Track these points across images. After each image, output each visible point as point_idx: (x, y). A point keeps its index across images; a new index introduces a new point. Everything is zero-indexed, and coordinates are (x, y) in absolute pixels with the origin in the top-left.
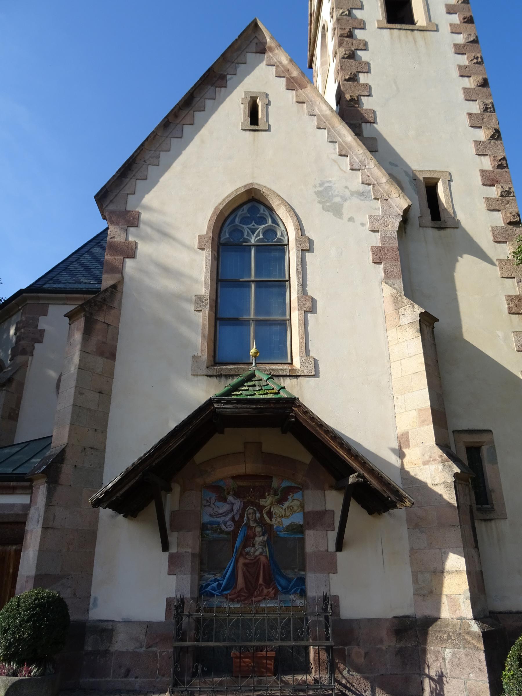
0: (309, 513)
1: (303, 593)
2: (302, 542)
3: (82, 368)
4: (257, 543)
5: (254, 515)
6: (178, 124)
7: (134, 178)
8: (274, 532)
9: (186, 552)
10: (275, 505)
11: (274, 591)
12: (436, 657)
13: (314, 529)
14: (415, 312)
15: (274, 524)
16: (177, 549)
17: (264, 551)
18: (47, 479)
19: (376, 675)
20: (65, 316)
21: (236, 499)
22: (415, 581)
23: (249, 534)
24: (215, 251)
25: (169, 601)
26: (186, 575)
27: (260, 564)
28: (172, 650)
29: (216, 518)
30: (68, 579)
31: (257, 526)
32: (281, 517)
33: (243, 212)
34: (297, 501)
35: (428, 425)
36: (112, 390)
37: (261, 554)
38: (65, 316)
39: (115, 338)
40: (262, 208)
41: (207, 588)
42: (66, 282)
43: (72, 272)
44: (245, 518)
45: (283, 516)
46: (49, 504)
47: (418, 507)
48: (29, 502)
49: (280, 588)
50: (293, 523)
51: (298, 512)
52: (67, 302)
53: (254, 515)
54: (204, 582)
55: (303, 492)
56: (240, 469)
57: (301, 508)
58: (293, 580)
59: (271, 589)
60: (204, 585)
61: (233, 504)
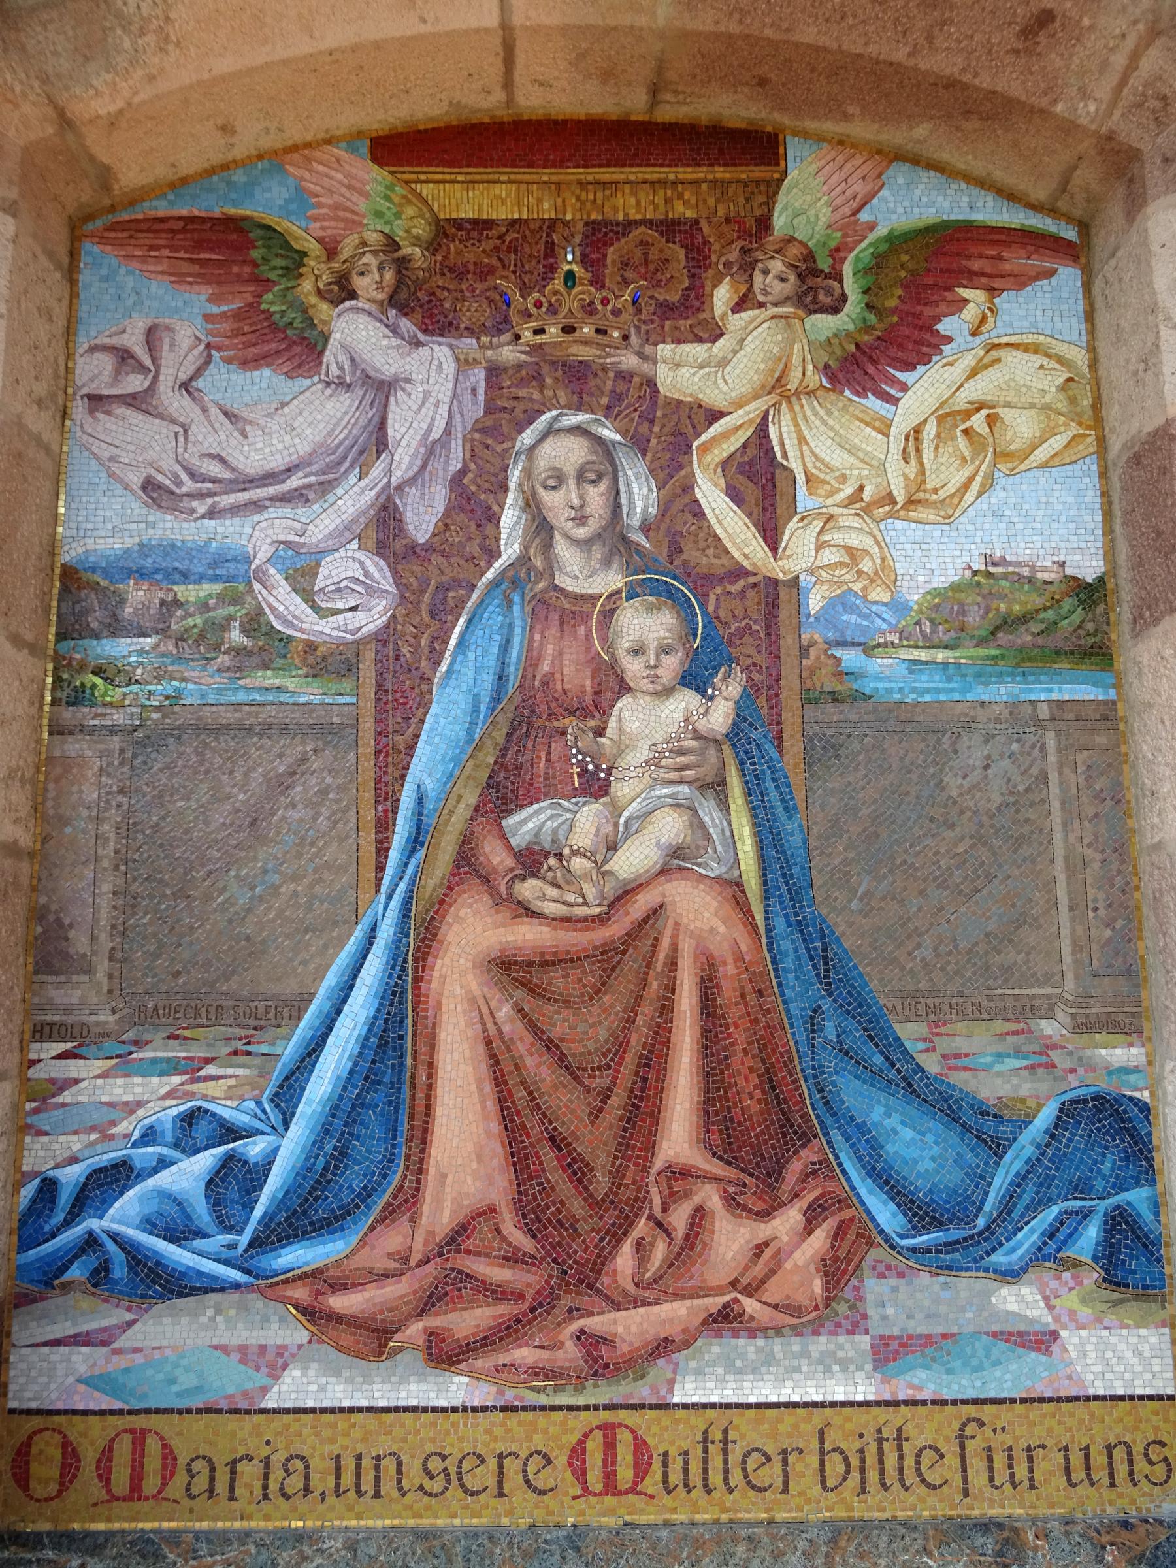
4: (638, 755)
5: (596, 497)
11: (820, 1239)
17: (708, 837)
23: (545, 667)
27: (672, 965)
29: (211, 514)
34: (1038, 360)
44: (510, 517)
45: (890, 499)
50: (1003, 562)
51: (1044, 466)
54: (76, 1144)
57: (1075, 430)
59: (791, 1218)
60: (71, 1176)
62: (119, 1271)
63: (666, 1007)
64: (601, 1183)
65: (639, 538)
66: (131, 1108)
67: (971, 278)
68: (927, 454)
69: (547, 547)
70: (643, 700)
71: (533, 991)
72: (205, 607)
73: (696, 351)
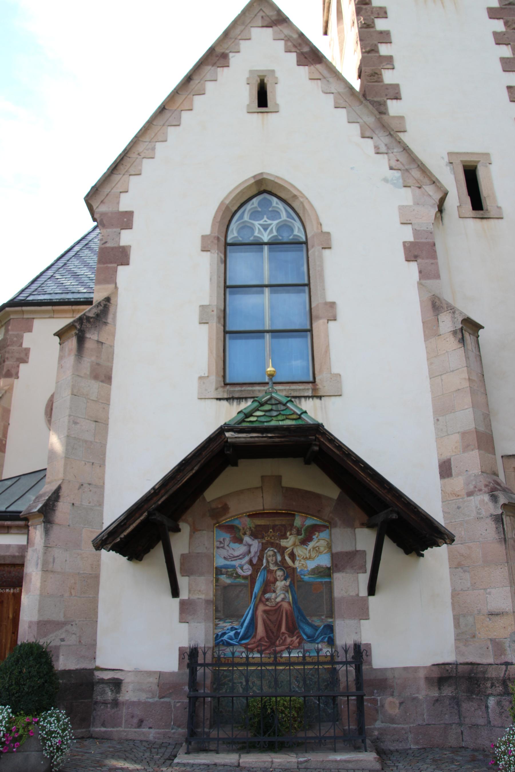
0: (337, 554)
1: (331, 642)
2: (330, 586)
3: (76, 394)
4: (279, 588)
5: (274, 558)
6: (175, 110)
7: (126, 173)
8: (297, 576)
9: (198, 598)
10: (298, 545)
11: (298, 640)
12: (479, 706)
13: (343, 572)
14: (456, 319)
15: (298, 567)
16: (189, 595)
17: (286, 597)
18: (44, 519)
19: (412, 725)
20: (55, 335)
21: (253, 540)
22: (457, 624)
23: (269, 578)
24: (221, 252)
25: (181, 650)
26: (200, 623)
27: (283, 611)
28: (188, 701)
29: (231, 561)
30: (72, 625)
31: (278, 569)
32: (306, 559)
33: (253, 206)
35: (473, 450)
36: (108, 418)
37: (283, 600)
38: (55, 335)
39: (110, 358)
40: (275, 200)
41: (223, 637)
42: (52, 292)
43: (59, 280)
44: (265, 561)
46: (47, 547)
47: (462, 544)
48: (25, 543)
49: (305, 637)
51: (324, 554)
52: (54, 315)
53: (274, 558)
54: (220, 630)
55: (330, 531)
56: (257, 506)
58: (320, 627)
59: (295, 638)
60: (220, 633)
61: (250, 546)
62: (225, 643)
63: (282, 616)
64: (275, 634)
65: (279, 563)
66: (226, 626)
67: (316, 531)
68: (311, 553)
69: (269, 564)
70: (280, 582)
71: (268, 614)
72: (231, 571)
73: (285, 540)
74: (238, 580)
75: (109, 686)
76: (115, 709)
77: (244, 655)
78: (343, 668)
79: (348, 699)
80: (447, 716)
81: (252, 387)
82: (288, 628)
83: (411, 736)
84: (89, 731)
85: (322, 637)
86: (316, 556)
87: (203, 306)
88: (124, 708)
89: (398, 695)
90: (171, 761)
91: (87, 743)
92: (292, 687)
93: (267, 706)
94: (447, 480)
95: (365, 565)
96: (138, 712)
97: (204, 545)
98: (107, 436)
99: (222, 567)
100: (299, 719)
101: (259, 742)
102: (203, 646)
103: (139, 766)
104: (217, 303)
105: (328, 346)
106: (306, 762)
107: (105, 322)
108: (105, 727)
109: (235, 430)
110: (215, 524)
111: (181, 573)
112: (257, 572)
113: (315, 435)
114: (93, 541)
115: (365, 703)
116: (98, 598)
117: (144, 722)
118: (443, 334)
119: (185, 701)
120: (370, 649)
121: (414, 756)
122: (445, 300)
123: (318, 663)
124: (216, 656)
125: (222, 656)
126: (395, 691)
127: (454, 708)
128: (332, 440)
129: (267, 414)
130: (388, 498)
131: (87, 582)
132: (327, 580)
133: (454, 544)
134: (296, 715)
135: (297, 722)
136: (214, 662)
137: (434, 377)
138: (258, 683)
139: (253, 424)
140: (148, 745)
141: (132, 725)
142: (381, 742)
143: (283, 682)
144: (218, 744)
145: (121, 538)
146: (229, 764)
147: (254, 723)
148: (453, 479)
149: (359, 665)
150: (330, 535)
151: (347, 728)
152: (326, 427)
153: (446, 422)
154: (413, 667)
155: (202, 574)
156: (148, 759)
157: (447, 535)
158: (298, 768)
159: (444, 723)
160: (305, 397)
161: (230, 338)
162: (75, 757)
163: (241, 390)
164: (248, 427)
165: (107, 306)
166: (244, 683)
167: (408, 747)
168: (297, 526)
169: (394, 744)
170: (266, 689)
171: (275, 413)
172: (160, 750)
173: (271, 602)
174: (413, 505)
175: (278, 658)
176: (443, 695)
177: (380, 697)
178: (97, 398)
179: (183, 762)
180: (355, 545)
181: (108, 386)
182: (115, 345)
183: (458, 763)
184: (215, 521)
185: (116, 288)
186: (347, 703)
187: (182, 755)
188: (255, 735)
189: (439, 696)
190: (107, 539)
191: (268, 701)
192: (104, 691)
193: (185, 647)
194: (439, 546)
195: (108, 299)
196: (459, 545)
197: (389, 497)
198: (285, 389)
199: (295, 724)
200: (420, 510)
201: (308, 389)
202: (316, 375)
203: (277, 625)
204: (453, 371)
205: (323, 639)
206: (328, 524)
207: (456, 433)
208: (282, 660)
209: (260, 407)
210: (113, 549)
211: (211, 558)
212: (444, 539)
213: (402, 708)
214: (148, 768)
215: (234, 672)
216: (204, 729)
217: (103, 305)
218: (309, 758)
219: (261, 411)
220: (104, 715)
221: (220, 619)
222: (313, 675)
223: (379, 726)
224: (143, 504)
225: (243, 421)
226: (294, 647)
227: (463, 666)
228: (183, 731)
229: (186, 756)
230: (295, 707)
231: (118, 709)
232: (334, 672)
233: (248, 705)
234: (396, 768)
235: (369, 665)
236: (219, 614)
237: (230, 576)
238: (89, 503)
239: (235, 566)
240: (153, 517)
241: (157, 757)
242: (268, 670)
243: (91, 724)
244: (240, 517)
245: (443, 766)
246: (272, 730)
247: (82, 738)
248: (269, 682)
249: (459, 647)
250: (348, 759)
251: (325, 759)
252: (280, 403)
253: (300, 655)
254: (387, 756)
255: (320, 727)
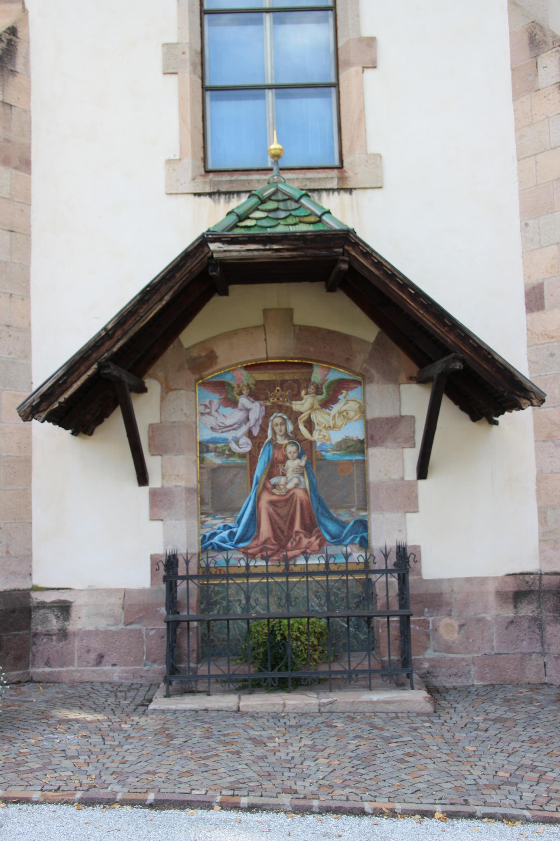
0: (374, 420)
1: (364, 543)
4: (290, 470)
5: (283, 428)
8: (316, 452)
9: (176, 486)
10: (318, 409)
11: (318, 541)
13: (382, 446)
15: (317, 440)
16: (162, 482)
19: (476, 655)
21: (253, 402)
22: (543, 519)
23: (276, 456)
25: (154, 560)
26: (179, 520)
27: (296, 501)
31: (289, 443)
37: (296, 486)
41: (213, 539)
47: (554, 407)
49: (328, 537)
51: (355, 420)
53: (283, 428)
54: (208, 530)
55: (364, 388)
58: (348, 523)
59: (313, 538)
60: (208, 535)
61: (248, 410)
62: (216, 547)
63: (295, 508)
64: (286, 534)
66: (216, 525)
67: (344, 388)
69: (275, 436)
71: (275, 506)
72: (222, 447)
73: (299, 402)
74: (232, 459)
75: (53, 611)
76: (64, 642)
77: (243, 563)
78: (381, 579)
79: (388, 621)
80: (524, 643)
81: (247, 175)
82: (303, 525)
83: (474, 670)
84: (28, 673)
85: (352, 536)
86: (342, 424)
87: (167, 44)
88: (76, 640)
89: (457, 614)
90: (145, 708)
91: (25, 688)
92: (310, 605)
93: (275, 631)
94: (536, 315)
95: (414, 437)
96: (97, 645)
97: (182, 410)
98: (30, 253)
99: (208, 442)
100: (321, 648)
101: (266, 679)
102: (185, 551)
103: (101, 715)
104: (191, 40)
105: (362, 110)
106: (331, 703)
107: (12, 71)
108: (50, 667)
109: (223, 239)
110: (197, 381)
111: (150, 451)
112: (259, 448)
113: (342, 247)
114: (18, 408)
115: (412, 626)
116: (31, 490)
117: (105, 657)
118: (543, 88)
119: (162, 627)
120: (419, 552)
121: (477, 694)
122: (551, 30)
123: (347, 572)
124: (203, 565)
125: (212, 565)
126: (453, 609)
127: (535, 633)
128: (369, 253)
129: (272, 215)
130: (450, 339)
131: (13, 468)
132: (359, 457)
133: (544, 408)
134: (316, 642)
135: (317, 652)
136: (201, 574)
137: (524, 158)
138: (263, 600)
139: (250, 231)
140: (112, 687)
141: (88, 662)
142: (433, 676)
143: (297, 598)
144: (209, 683)
145: (60, 403)
146: (225, 709)
147: (258, 654)
148: (545, 313)
149: (404, 575)
150: (364, 394)
151: (386, 658)
152: (359, 234)
153: (539, 228)
154: (479, 578)
155: (180, 452)
156: (113, 706)
157: (534, 393)
158: (319, 712)
159: (521, 652)
160: (327, 190)
161: (212, 100)
162: (9, 708)
163: (231, 181)
164: (244, 236)
165: (13, 43)
166: (244, 602)
167: (470, 683)
168: (316, 381)
169: (451, 680)
170: (274, 609)
171: (282, 214)
172: (128, 694)
173: (280, 489)
174: (486, 351)
175: (291, 566)
176: (521, 615)
177: (433, 618)
178: (10, 194)
179: (161, 708)
180: (400, 408)
181: (26, 175)
182: (32, 110)
183: (539, 704)
184: (197, 376)
185: (24, 10)
186: (386, 625)
187: (159, 699)
188: (260, 671)
189: (515, 617)
190: (38, 404)
191: (278, 625)
192: (47, 618)
193: (159, 554)
194: (521, 408)
195: (13, 31)
196: (550, 409)
197: (450, 338)
198: (297, 179)
199: (315, 654)
200: (496, 357)
201: (332, 178)
202: (344, 157)
203: (288, 522)
204: (554, 148)
205: (353, 540)
206: (360, 378)
207: (554, 244)
208: (296, 569)
209: (260, 205)
210: (49, 418)
211: (193, 429)
212: (530, 399)
213: (462, 632)
214: (114, 717)
215: (229, 587)
216: (189, 664)
217: (6, 41)
218: (335, 699)
219: (262, 211)
220: (48, 651)
221: (208, 515)
222: (339, 589)
223: (431, 657)
224: (90, 352)
225: (236, 226)
226: (312, 551)
227: (549, 577)
228: (161, 667)
229: (166, 699)
230: (315, 632)
231: (67, 642)
232: (368, 584)
233: (249, 631)
234: (453, 711)
235: (417, 575)
236: (205, 508)
237: (220, 453)
238: (10, 354)
239: (228, 439)
240: (106, 372)
241: (124, 703)
242: (277, 582)
243: (31, 663)
244: (233, 370)
245: (518, 708)
246: (282, 663)
247: (19, 682)
248: (278, 599)
249: (545, 551)
250: (388, 699)
251: (357, 700)
252: (291, 198)
253: (321, 562)
254: (441, 695)
255: (349, 658)
